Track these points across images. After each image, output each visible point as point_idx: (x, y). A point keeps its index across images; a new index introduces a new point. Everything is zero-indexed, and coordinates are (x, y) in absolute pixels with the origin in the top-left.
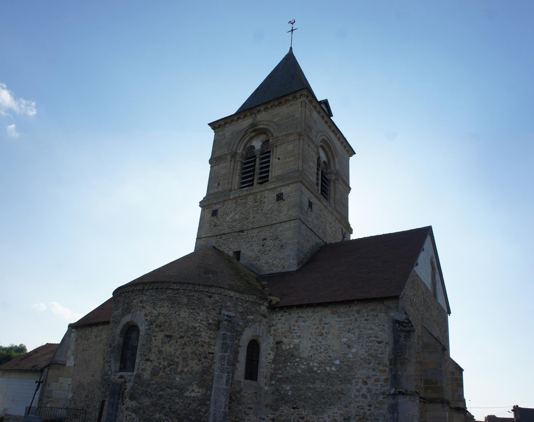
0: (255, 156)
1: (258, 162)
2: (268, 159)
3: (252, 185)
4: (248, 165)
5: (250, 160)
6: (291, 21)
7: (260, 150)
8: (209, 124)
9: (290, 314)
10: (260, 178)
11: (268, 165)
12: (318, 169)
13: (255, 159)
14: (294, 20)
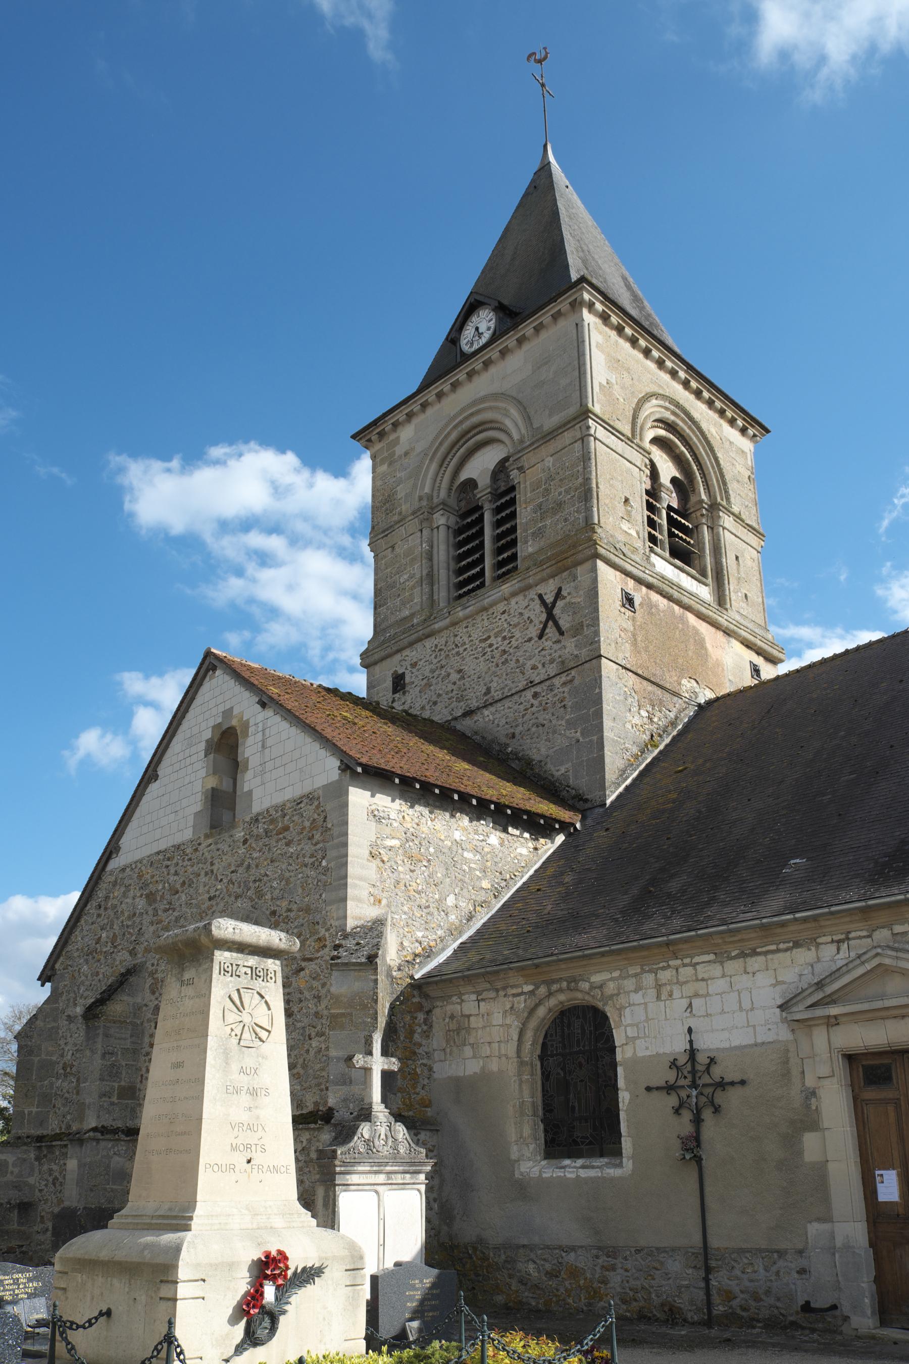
0: (479, 508)
1: (488, 517)
2: (512, 509)
3: (483, 585)
4: (470, 560)
5: (469, 533)
6: (534, 54)
7: (489, 490)
8: (354, 437)
9: (452, 816)
10: (498, 538)
11: (513, 554)
12: (651, 507)
13: (480, 528)
14: (545, 48)
